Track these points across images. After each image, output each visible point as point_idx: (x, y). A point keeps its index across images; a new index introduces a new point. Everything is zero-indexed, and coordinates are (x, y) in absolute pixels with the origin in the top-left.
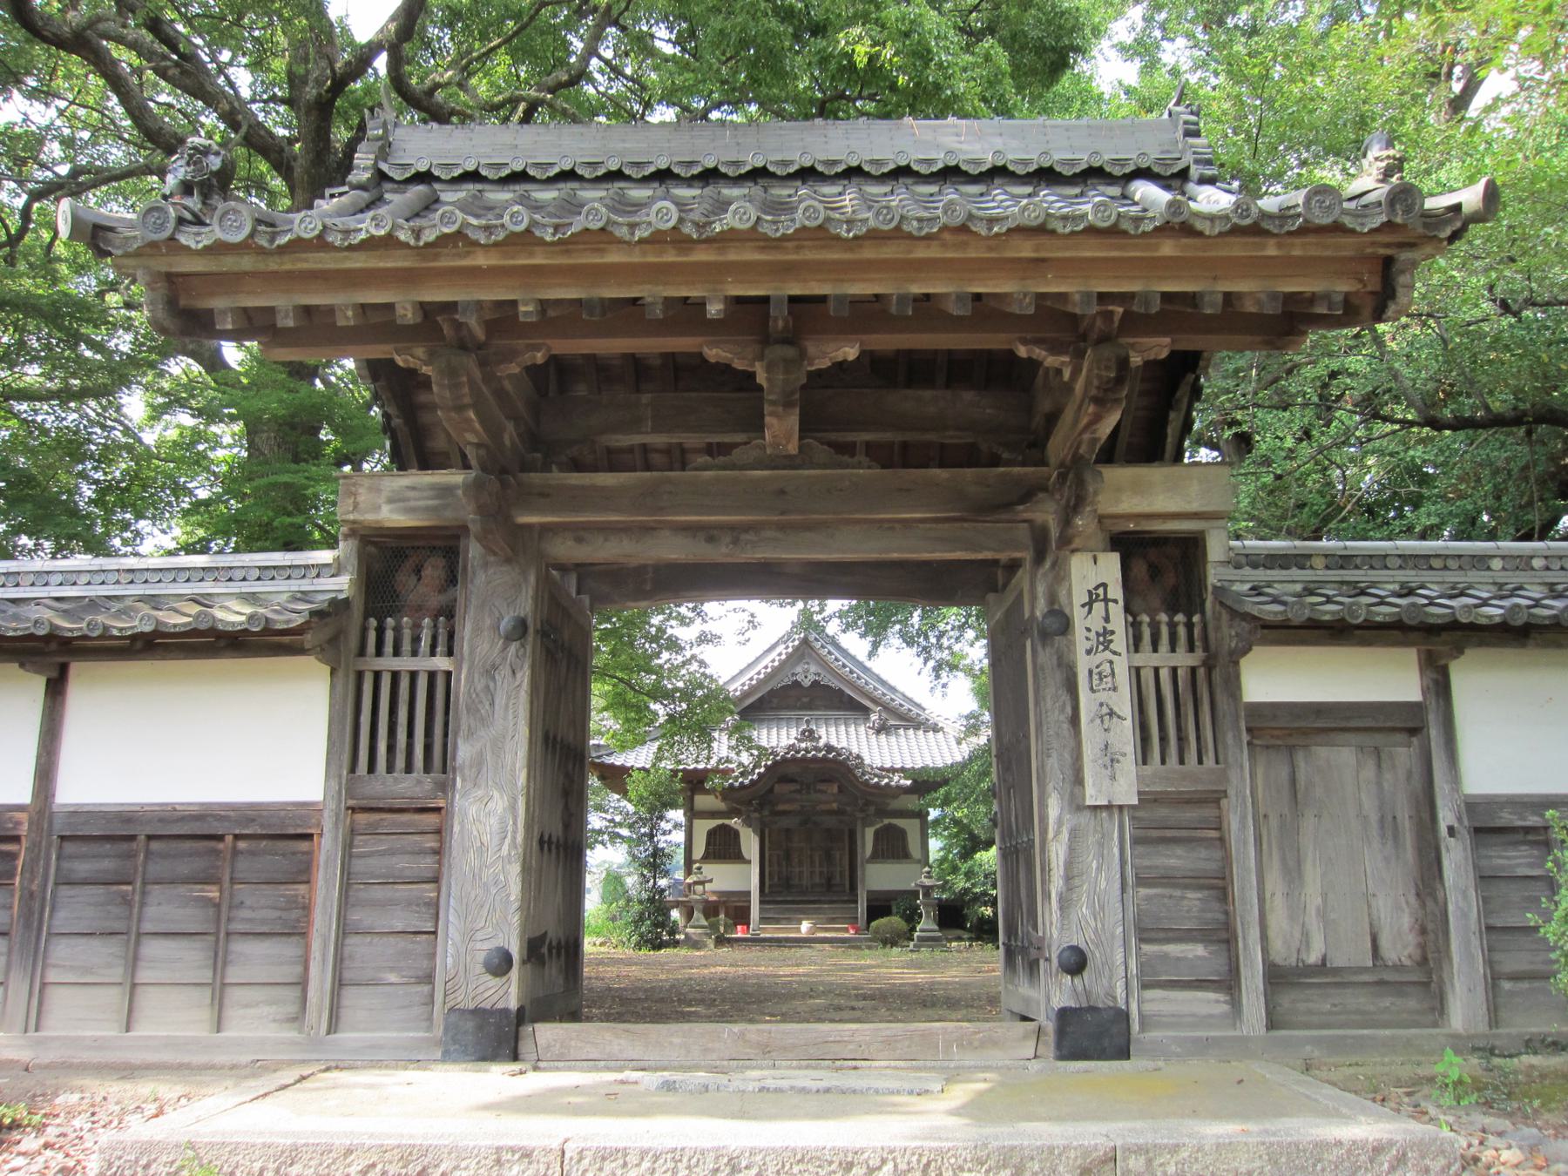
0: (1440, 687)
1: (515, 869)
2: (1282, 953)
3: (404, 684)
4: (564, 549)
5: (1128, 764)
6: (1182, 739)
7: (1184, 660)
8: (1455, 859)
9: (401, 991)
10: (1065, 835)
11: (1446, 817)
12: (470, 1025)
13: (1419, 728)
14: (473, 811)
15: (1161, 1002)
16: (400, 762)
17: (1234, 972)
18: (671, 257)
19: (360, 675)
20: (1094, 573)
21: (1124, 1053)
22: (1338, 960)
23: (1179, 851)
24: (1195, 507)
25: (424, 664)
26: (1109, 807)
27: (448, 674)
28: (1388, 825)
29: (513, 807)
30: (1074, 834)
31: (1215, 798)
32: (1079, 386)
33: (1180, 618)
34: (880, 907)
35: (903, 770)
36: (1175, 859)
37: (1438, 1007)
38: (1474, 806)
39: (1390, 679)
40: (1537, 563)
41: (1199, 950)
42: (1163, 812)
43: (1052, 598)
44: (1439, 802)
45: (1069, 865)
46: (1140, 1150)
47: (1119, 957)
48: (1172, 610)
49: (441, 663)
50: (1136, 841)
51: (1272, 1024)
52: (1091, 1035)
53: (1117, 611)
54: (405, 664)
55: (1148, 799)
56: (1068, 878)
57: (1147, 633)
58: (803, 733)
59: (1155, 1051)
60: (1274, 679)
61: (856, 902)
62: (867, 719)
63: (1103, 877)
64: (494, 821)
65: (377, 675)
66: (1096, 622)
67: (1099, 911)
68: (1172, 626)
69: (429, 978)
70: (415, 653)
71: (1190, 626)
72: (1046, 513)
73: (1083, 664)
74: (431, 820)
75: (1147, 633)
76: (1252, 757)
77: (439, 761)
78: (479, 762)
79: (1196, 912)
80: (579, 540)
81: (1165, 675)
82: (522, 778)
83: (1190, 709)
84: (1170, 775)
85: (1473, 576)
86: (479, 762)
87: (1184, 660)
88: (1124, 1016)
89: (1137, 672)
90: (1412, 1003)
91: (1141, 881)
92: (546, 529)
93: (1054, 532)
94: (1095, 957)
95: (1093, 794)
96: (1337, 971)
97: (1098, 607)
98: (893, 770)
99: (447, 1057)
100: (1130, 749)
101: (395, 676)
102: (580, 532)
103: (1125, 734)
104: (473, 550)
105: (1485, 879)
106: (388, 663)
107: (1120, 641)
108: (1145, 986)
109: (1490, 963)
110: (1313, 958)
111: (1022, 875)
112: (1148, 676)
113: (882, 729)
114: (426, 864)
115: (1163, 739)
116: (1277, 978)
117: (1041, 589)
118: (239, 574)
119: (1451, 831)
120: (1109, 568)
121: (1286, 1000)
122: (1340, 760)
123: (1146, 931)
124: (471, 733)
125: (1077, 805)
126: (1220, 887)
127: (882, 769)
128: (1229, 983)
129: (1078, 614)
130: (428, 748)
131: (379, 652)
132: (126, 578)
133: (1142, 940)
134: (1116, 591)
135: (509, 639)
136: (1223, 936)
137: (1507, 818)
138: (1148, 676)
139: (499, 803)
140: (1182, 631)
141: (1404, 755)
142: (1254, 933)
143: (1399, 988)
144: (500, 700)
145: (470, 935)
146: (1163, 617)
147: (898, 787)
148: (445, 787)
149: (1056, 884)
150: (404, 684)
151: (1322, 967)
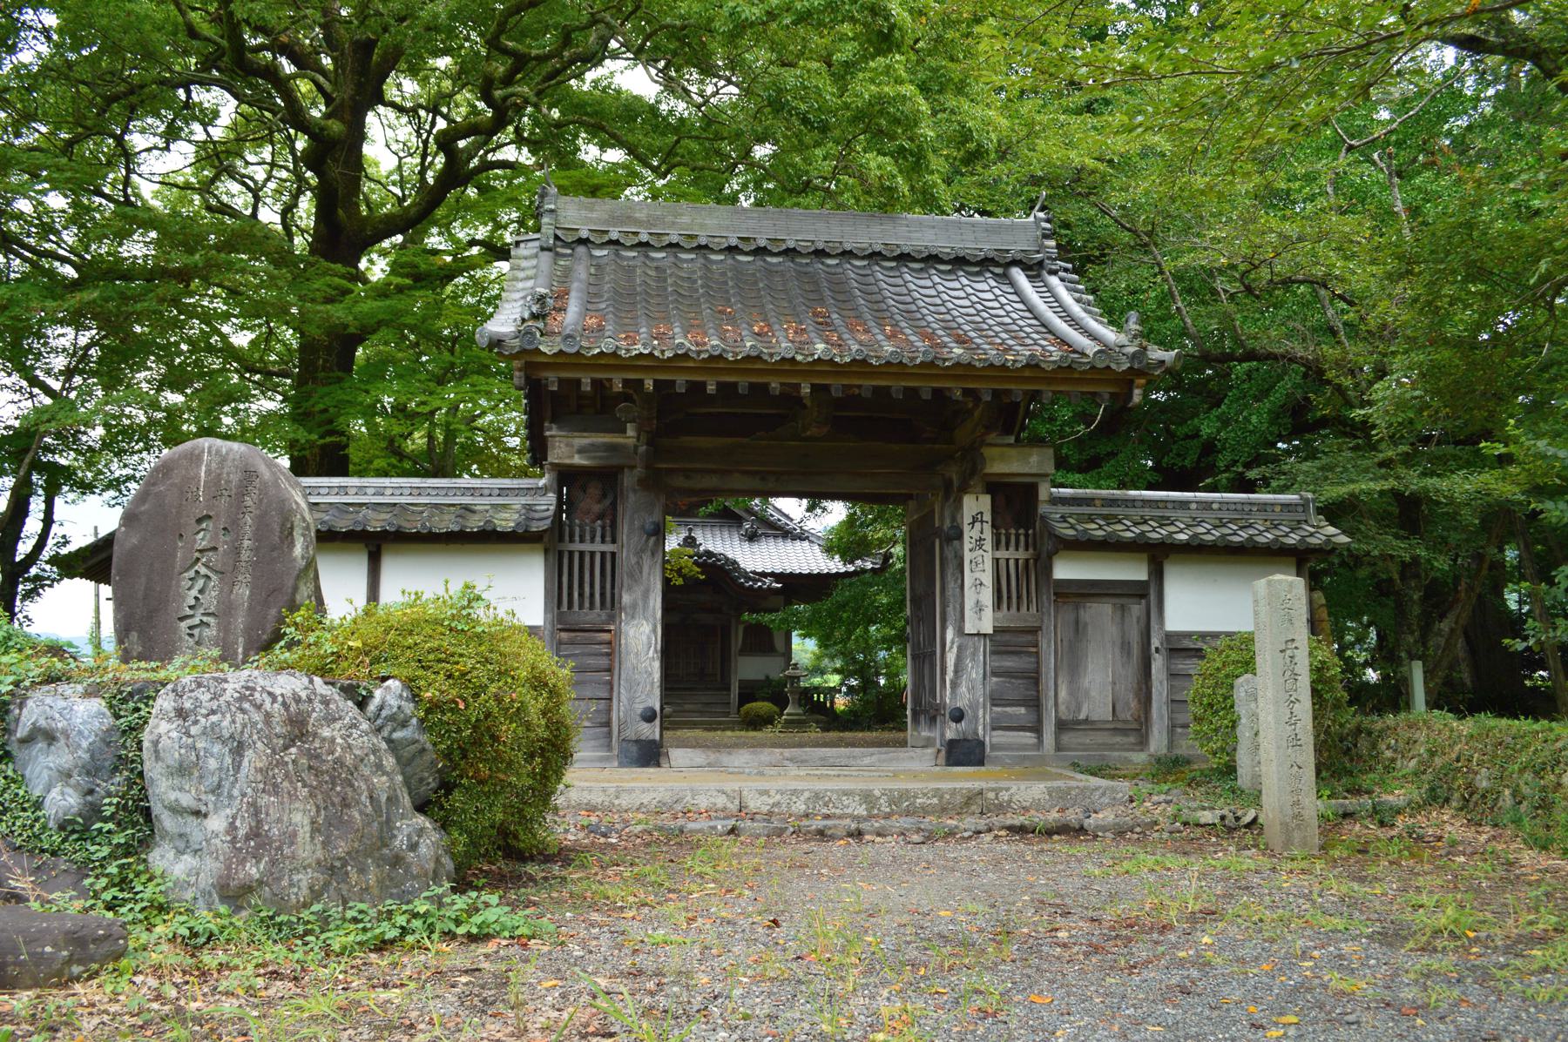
0: (1158, 575)
1: (657, 664)
2: (1065, 714)
3: (587, 559)
4: (679, 482)
5: (988, 614)
6: (1019, 597)
7: (1022, 555)
8: (1158, 663)
9: (592, 731)
10: (955, 650)
11: (1155, 642)
12: (634, 749)
13: (1147, 595)
14: (631, 632)
15: (1000, 737)
16: (587, 604)
17: (1040, 721)
18: (787, 367)
19: (561, 554)
20: (976, 505)
21: (981, 763)
22: (1094, 717)
23: (1016, 658)
24: (1034, 471)
25: (598, 547)
26: (978, 634)
27: (613, 554)
28: (1125, 647)
29: (654, 631)
30: (959, 648)
31: (1034, 631)
32: (977, 414)
33: (1021, 531)
34: (749, 692)
35: (772, 574)
36: (1009, 663)
37: (1143, 743)
38: (1170, 636)
39: (1133, 571)
40: (1215, 506)
41: (1023, 710)
42: (1007, 637)
43: (954, 519)
44: (1153, 634)
45: (956, 665)
46: (993, 790)
47: (981, 713)
48: (1018, 526)
49: (608, 548)
50: (993, 653)
51: (1058, 748)
52: (964, 753)
53: (987, 528)
54: (587, 547)
55: (996, 630)
56: (956, 672)
57: (1003, 539)
58: (685, 539)
59: (997, 761)
60: (1064, 570)
61: (729, 689)
62: (740, 526)
63: (974, 672)
64: (644, 638)
65: (571, 553)
66: (975, 533)
67: (971, 689)
68: (1018, 536)
69: (608, 724)
70: (582, 541)
71: (1027, 536)
72: (953, 473)
73: (968, 556)
74: (606, 636)
75: (1003, 539)
76: (1056, 612)
77: (611, 603)
78: (634, 606)
79: (1022, 688)
80: (687, 477)
81: (1012, 563)
82: (659, 614)
83: (1024, 582)
84: (1010, 618)
85: (1179, 513)
86: (634, 606)
87: (1022, 555)
88: (982, 744)
89: (996, 561)
90: (1132, 739)
91: (994, 674)
92: (672, 471)
93: (956, 483)
94: (969, 713)
95: (969, 628)
96: (1093, 722)
97: (978, 525)
98: (764, 575)
99: (621, 765)
100: (990, 603)
101: (582, 554)
102: (687, 473)
103: (987, 596)
104: (628, 480)
105: (1173, 676)
106: (577, 546)
107: (988, 545)
108: (994, 729)
109: (1171, 719)
110: (1082, 716)
111: (927, 672)
112: (1002, 563)
113: (752, 537)
114: (604, 662)
115: (1009, 598)
116: (1062, 726)
117: (947, 513)
118: (487, 492)
119: (1157, 650)
120: (986, 500)
121: (1067, 738)
122: (1101, 614)
123: (996, 700)
124: (630, 589)
125: (960, 631)
126: (1034, 678)
127: (754, 572)
128: (1037, 729)
129: (966, 528)
130: (603, 595)
131: (572, 540)
132: (415, 492)
133: (993, 705)
134: (987, 517)
135: (650, 535)
136: (1035, 704)
137: (1187, 644)
138: (1002, 563)
139: (646, 628)
140: (1022, 538)
141: (1136, 609)
142: (1051, 702)
143: (1124, 732)
144: (646, 569)
145: (631, 700)
146: (1013, 531)
147: (770, 589)
148: (612, 618)
149: (950, 675)
150: (587, 559)
151: (1086, 721)
